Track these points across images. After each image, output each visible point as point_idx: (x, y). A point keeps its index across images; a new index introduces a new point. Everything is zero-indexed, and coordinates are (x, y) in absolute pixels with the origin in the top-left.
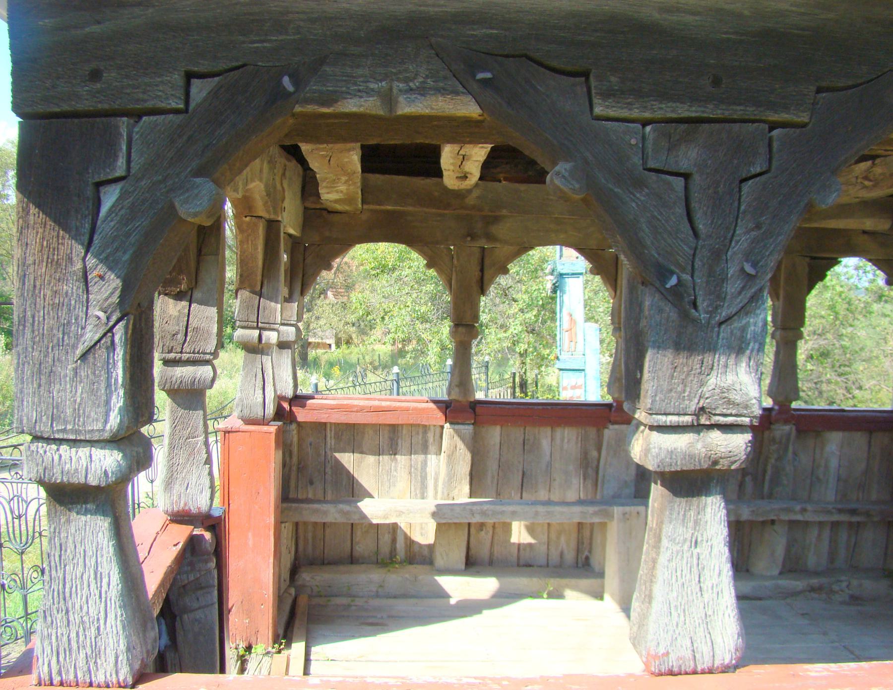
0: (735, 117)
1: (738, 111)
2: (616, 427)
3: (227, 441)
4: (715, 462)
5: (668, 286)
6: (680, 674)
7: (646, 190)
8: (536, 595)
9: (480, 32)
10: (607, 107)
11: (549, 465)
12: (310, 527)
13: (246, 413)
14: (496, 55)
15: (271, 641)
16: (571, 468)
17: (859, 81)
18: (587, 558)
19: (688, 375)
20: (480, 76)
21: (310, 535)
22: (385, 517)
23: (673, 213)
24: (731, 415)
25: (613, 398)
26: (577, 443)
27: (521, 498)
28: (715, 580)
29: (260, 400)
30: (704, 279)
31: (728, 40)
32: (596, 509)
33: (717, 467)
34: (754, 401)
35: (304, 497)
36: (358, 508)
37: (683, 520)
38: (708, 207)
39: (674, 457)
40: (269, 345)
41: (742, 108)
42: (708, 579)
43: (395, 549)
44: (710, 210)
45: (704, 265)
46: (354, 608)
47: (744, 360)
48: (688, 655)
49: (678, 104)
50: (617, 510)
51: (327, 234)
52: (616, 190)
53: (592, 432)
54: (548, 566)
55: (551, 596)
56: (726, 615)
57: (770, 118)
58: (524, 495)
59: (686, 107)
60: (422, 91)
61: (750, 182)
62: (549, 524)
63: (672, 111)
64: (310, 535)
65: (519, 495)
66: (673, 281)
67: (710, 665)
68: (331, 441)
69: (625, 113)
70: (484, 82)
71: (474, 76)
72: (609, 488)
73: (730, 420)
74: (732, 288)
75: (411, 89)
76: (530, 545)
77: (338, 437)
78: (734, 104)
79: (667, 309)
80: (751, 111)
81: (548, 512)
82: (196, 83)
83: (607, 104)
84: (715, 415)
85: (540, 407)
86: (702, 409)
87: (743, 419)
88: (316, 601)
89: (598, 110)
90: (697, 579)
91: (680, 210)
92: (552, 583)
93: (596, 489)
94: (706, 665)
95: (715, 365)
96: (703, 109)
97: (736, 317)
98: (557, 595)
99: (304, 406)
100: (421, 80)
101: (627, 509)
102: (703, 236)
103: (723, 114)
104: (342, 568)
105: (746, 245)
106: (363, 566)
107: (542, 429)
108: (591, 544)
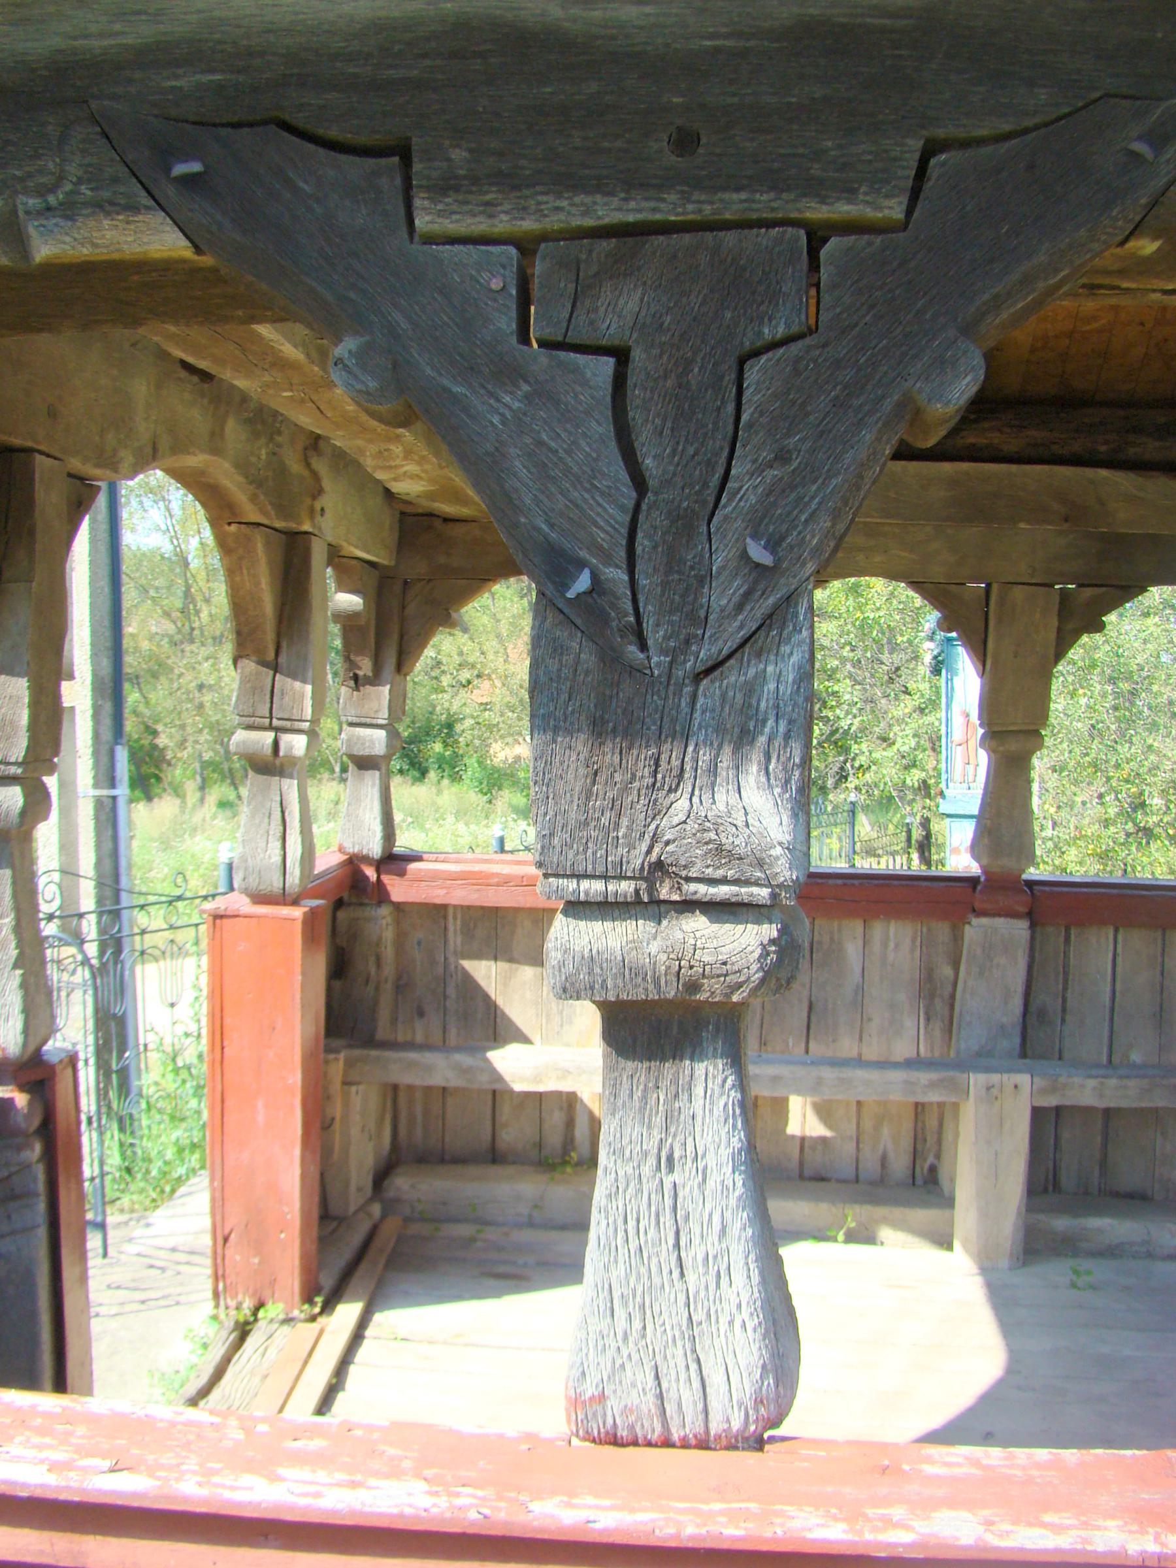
0: (727, 216)
1: (733, 204)
2: (984, 921)
3: (218, 935)
4: (693, 986)
5: (570, 595)
6: (635, 1443)
7: (526, 388)
8: (821, 1236)
9: (186, 80)
10: (440, 214)
11: (860, 990)
12: (418, 1095)
13: (253, 882)
14: (215, 125)
15: (297, 1298)
16: (902, 997)
17: (1029, 122)
18: (933, 1169)
19: (626, 789)
20: (180, 169)
21: (419, 1109)
22: (537, 1079)
23: (584, 435)
24: (724, 881)
25: (981, 867)
26: (912, 951)
27: (807, 1052)
28: (713, 1244)
29: (277, 858)
30: (657, 579)
31: (717, 50)
32: (934, 1076)
33: (702, 996)
34: (778, 851)
35: (409, 1038)
36: (487, 1061)
37: (642, 1110)
38: (665, 420)
39: (597, 970)
40: (293, 761)
41: (743, 196)
42: (696, 1240)
43: (572, 1140)
44: (669, 424)
45: (655, 547)
46: (479, 1244)
47: (756, 756)
48: (649, 1402)
49: (598, 198)
50: (977, 1081)
51: (442, 560)
52: (457, 389)
53: (942, 930)
54: (857, 1180)
55: (851, 1238)
56: (738, 1324)
57: (808, 215)
58: (811, 1045)
59: (615, 202)
60: (69, 210)
61: (764, 358)
62: (859, 1103)
63: (585, 214)
64: (419, 1109)
65: (803, 1045)
66: (583, 582)
67: (699, 1428)
68: (455, 938)
69: (478, 225)
70: (189, 181)
71: (168, 170)
72: (970, 1039)
73: (723, 891)
74: (721, 596)
75: (49, 209)
76: (823, 1140)
77: (468, 932)
78: (725, 189)
79: (575, 645)
80: (764, 203)
81: (841, 1080)
82: (607, 365)
83: (440, 207)
84: (688, 879)
85: (839, 882)
86: (659, 865)
87: (755, 890)
88: (415, 1229)
89: (422, 222)
90: (671, 1241)
91: (602, 427)
92: (853, 1216)
93: (950, 1039)
94: (692, 1426)
95: (688, 767)
96: (652, 204)
97: (732, 662)
98: (863, 1236)
99: (402, 873)
100: (68, 187)
101: (995, 1078)
102: (651, 483)
103: (700, 211)
104: (473, 1170)
105: (753, 499)
106: (510, 1170)
107: (845, 922)
108: (939, 1142)
